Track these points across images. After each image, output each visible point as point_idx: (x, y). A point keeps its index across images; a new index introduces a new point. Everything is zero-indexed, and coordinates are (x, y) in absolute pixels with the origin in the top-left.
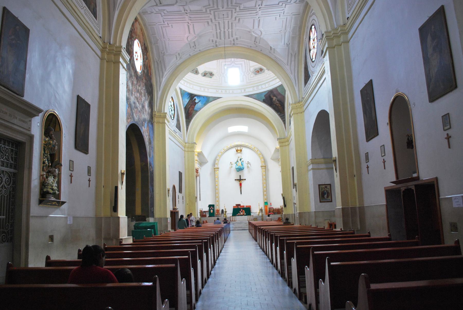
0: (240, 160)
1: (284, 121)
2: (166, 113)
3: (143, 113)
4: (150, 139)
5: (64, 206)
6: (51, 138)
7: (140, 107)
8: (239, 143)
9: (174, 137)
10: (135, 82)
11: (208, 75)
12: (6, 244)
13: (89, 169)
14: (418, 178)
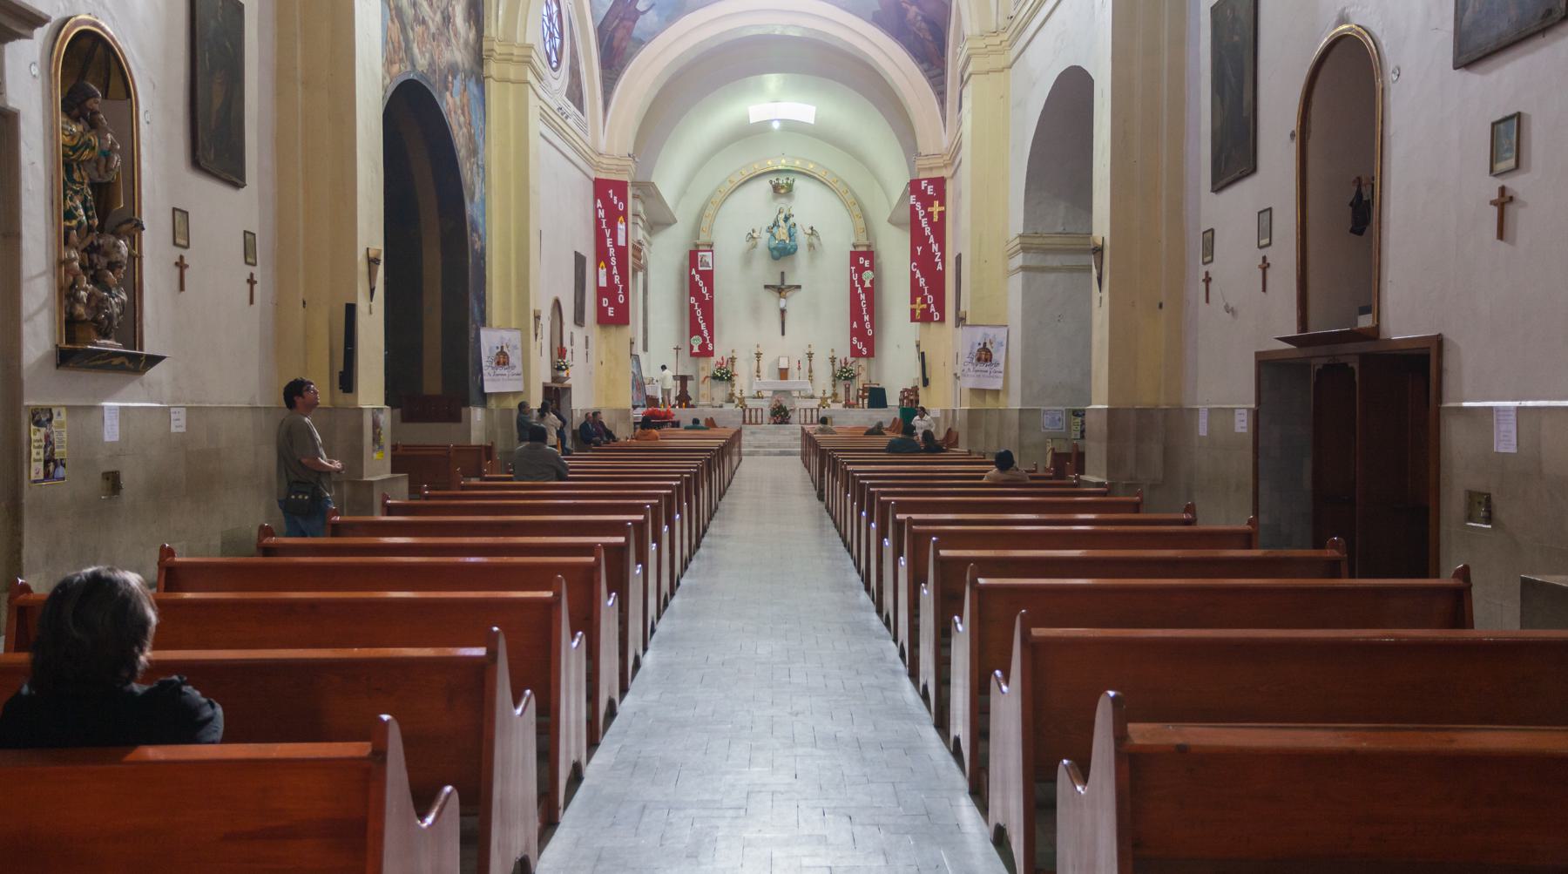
0: (786, 219)
1: (941, 95)
2: (531, 47)
3: (448, 43)
4: (471, 137)
5: (154, 373)
6: (93, 124)
7: (434, 20)
8: (782, 164)
9: (560, 132)
13: (249, 240)
14: (1373, 334)
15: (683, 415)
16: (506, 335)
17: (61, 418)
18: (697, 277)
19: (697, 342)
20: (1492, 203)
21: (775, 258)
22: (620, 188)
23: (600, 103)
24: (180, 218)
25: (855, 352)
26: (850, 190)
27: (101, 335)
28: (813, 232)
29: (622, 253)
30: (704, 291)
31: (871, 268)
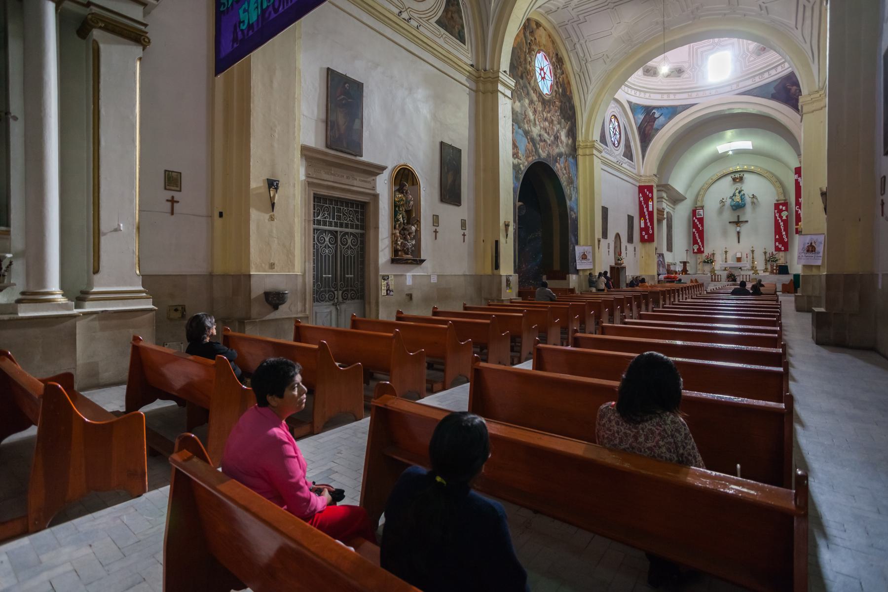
0: (740, 192)
3: (557, 146)
8: (738, 168)
10: (540, 109)
12: (356, 301)
15: (685, 278)
16: (586, 248)
17: (391, 278)
19: (696, 247)
20: (178, 202)
21: (734, 210)
22: (650, 188)
23: (641, 156)
24: (436, 220)
26: (774, 175)
27: (406, 254)
29: (651, 214)
31: (787, 210)
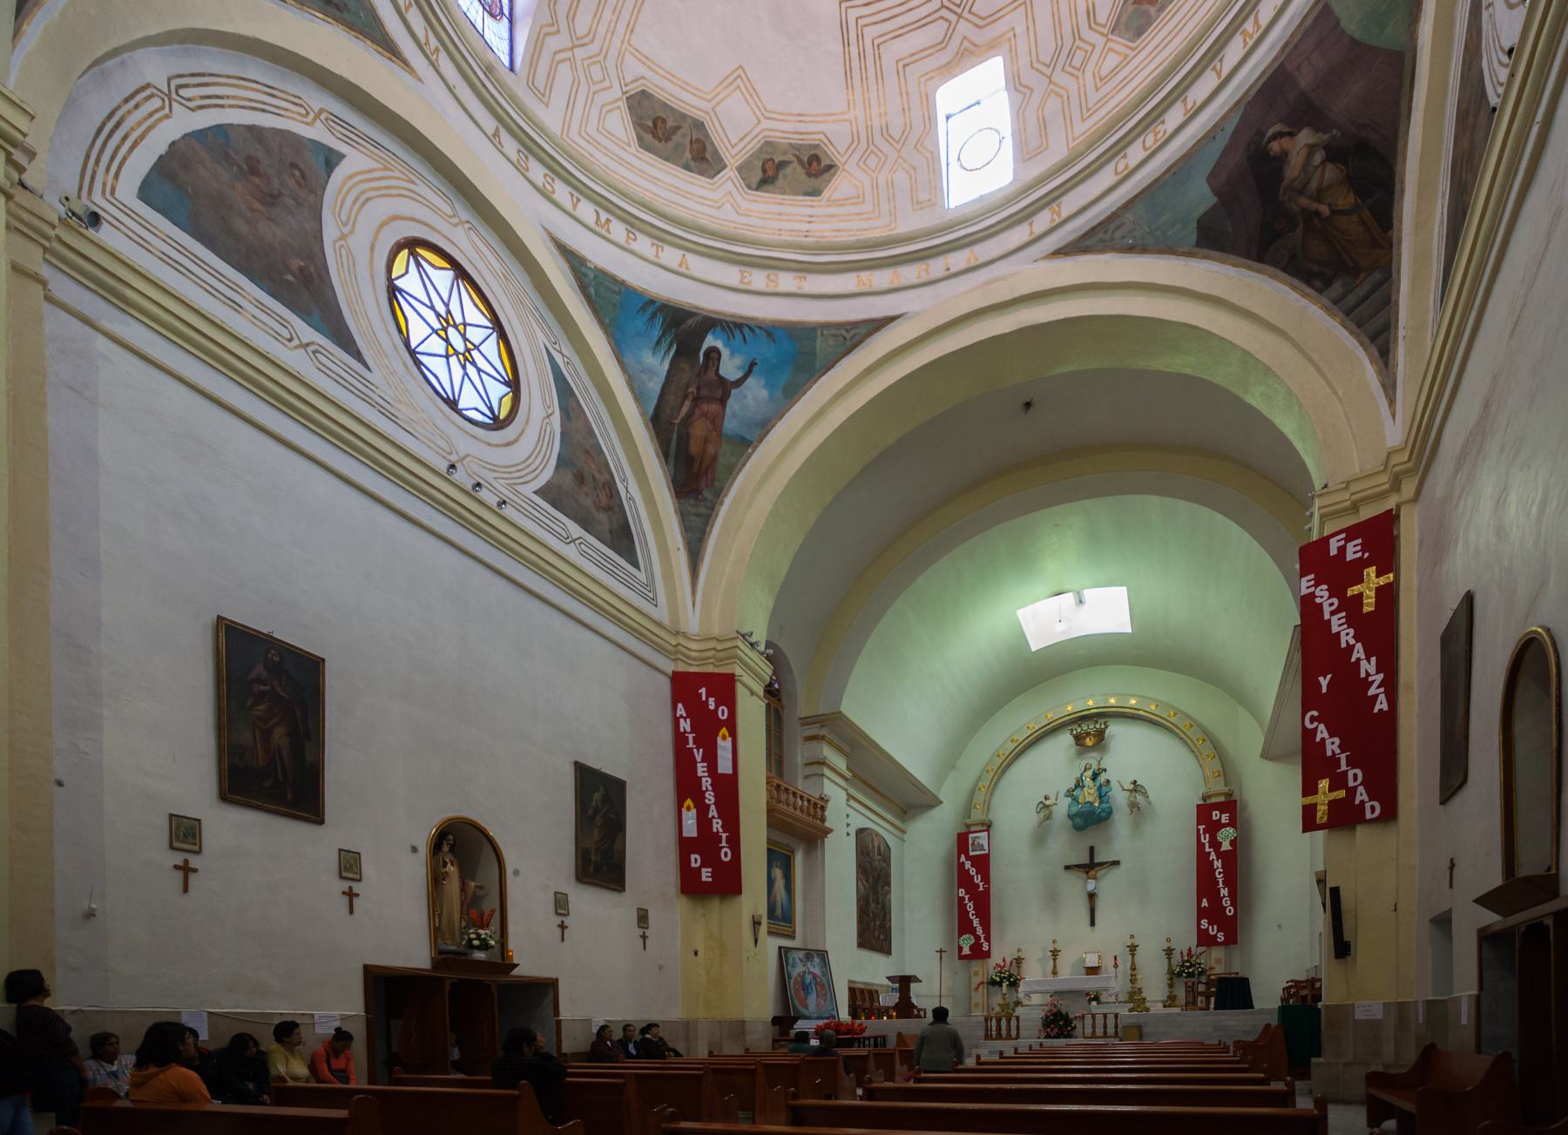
0: (1095, 776)
11: (795, 171)
18: (968, 865)
19: (967, 942)
20: (195, 871)
23: (681, 559)
25: (1204, 939)
28: (1136, 787)
30: (978, 880)
31: (1233, 823)
